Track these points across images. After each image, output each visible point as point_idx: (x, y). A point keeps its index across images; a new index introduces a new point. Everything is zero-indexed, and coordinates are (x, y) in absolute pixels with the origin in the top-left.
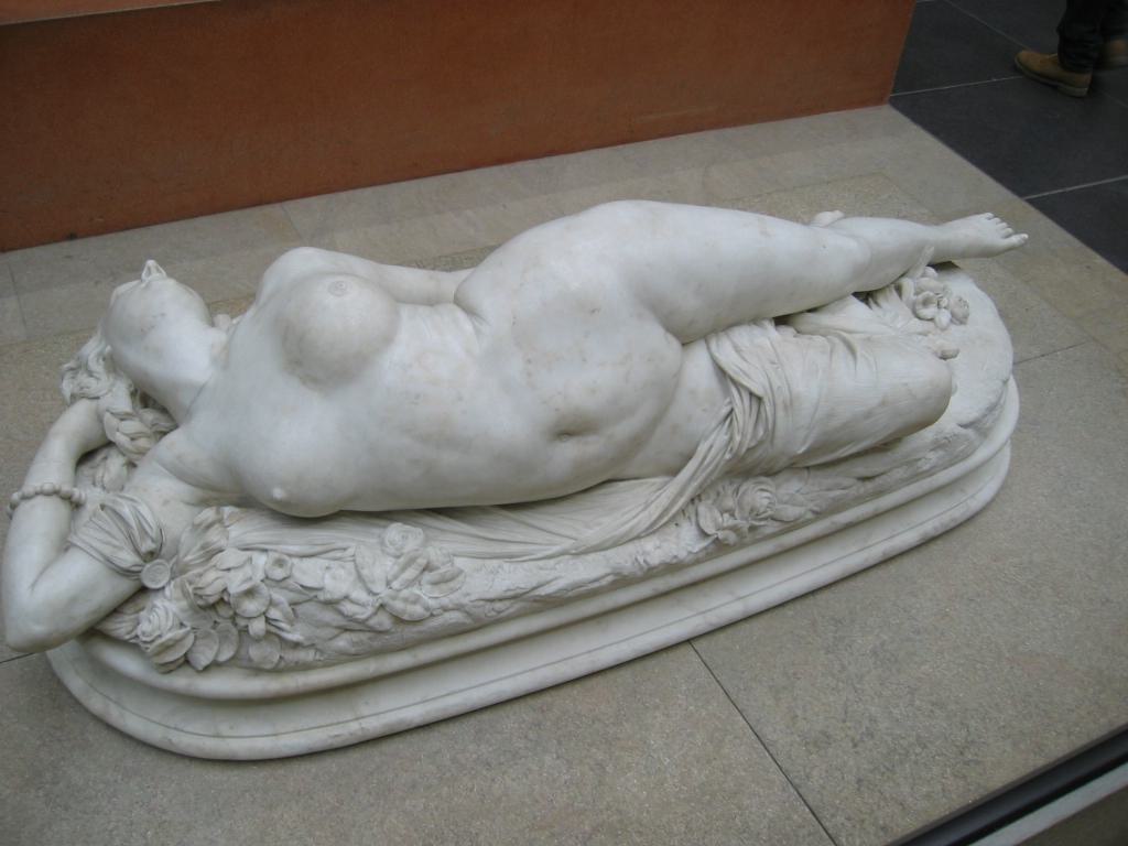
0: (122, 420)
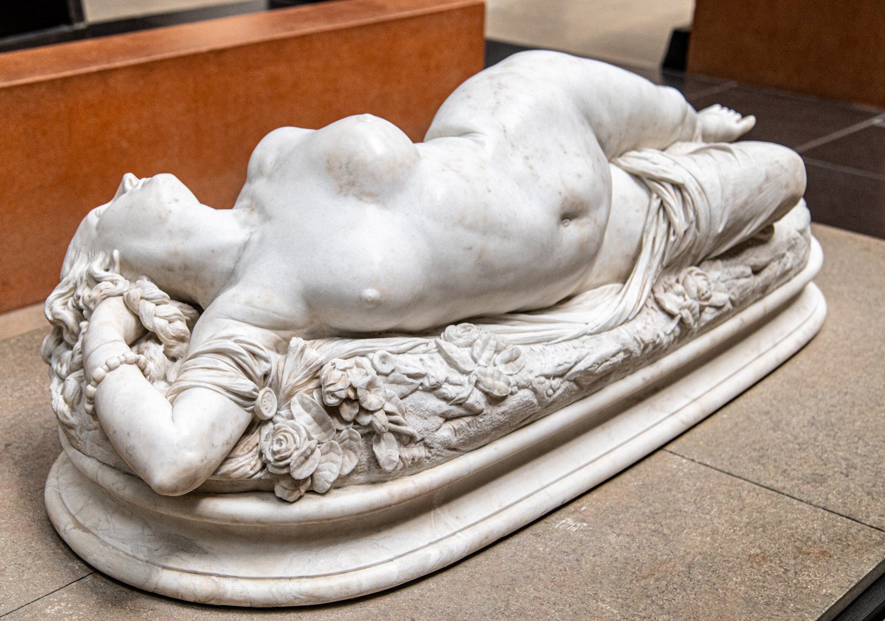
0: (157, 305)
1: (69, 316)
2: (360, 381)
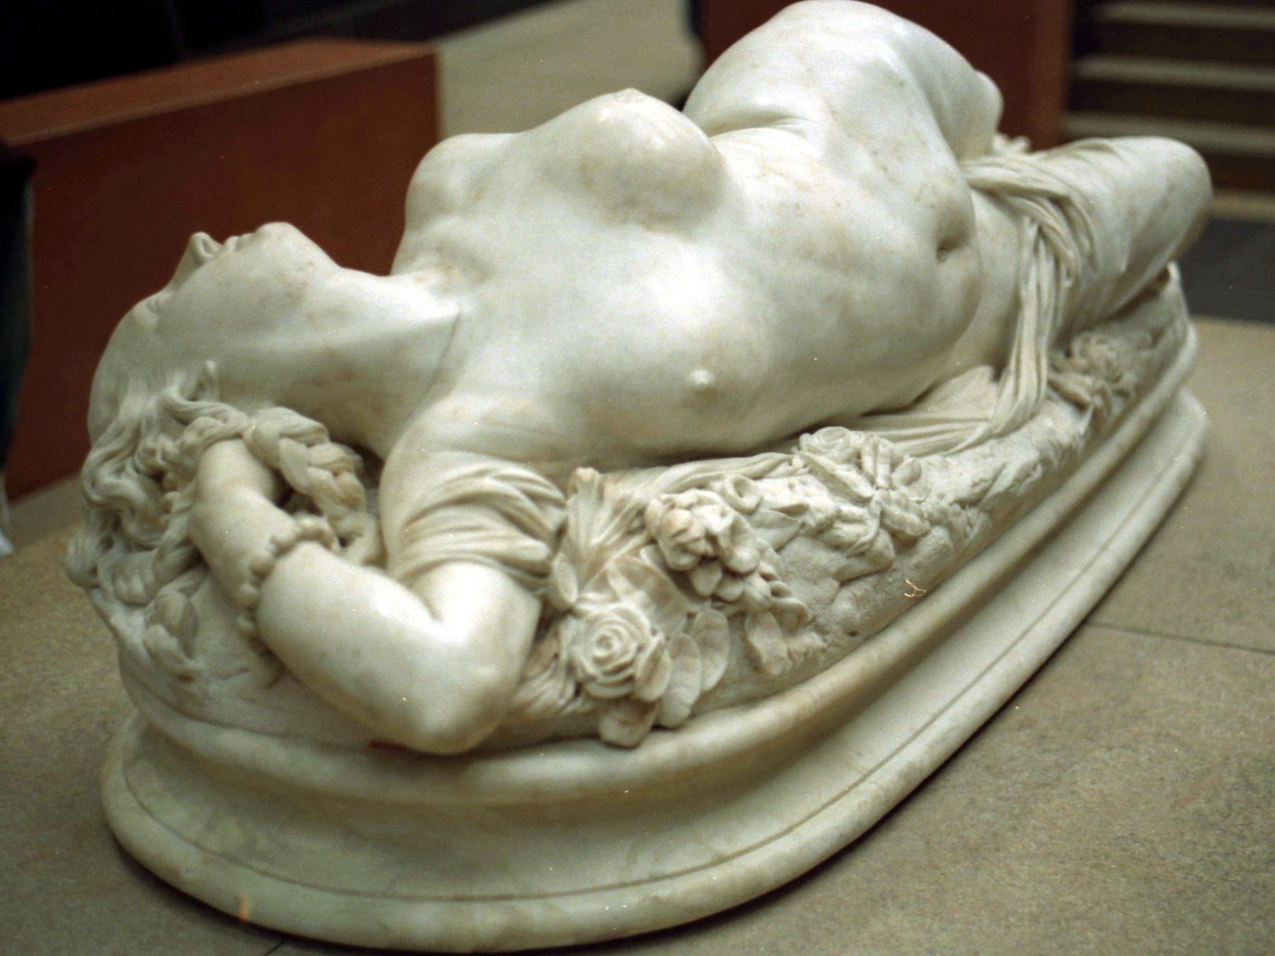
1: (131, 486)
2: (719, 525)
